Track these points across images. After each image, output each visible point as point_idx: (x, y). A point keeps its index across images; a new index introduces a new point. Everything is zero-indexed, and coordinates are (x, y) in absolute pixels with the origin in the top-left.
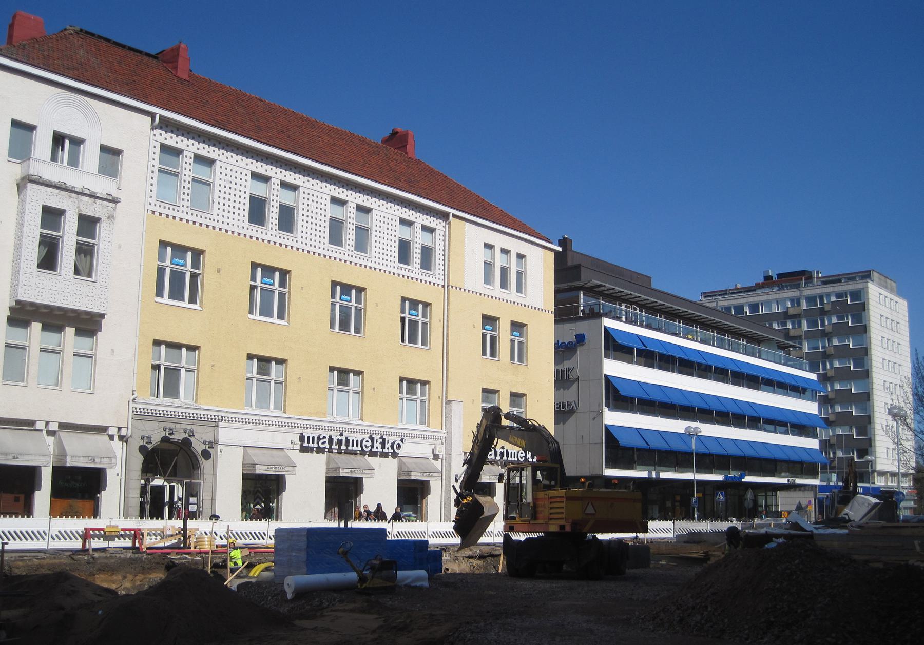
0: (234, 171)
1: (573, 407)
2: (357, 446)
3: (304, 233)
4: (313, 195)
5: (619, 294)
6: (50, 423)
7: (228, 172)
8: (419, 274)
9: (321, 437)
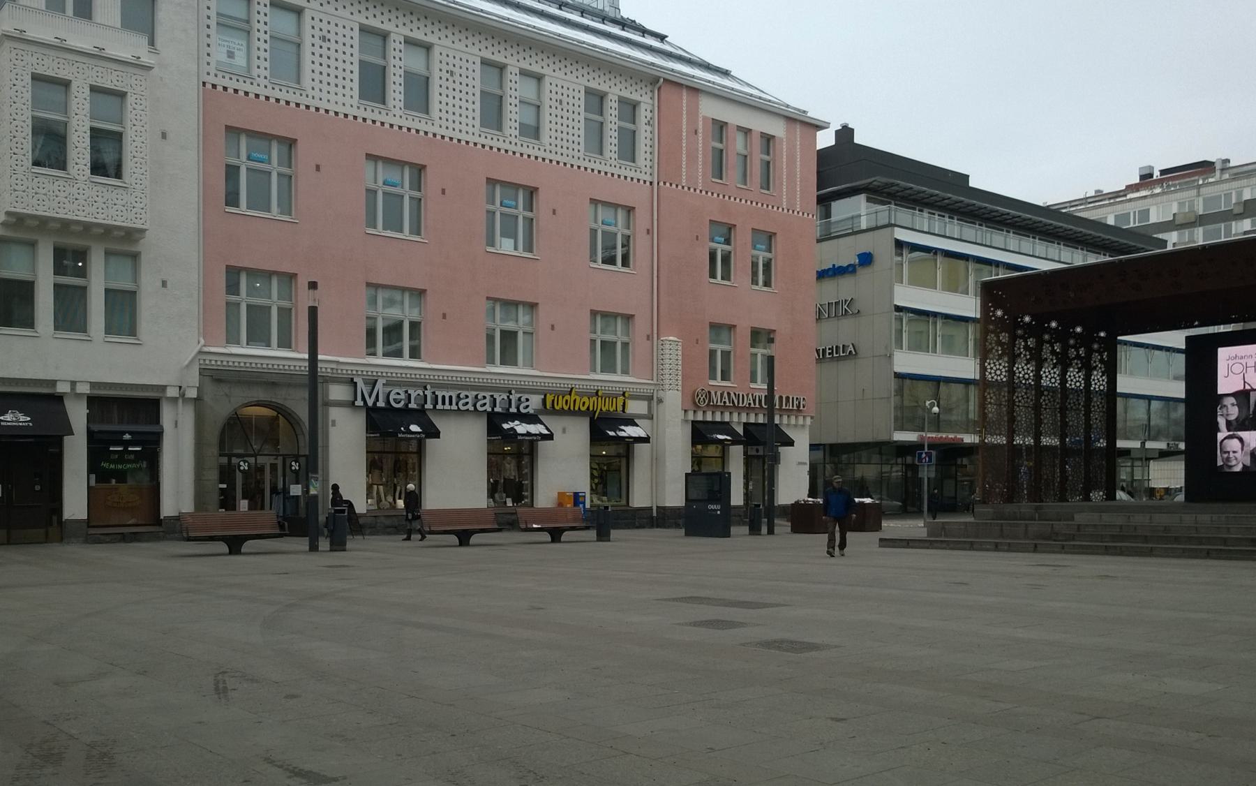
0: (325, 22)
1: (850, 351)
2: (451, 404)
3: (444, 111)
4: (562, 87)
5: (957, 204)
6: (168, 388)
7: (450, 60)
8: (615, 166)
9: (461, 396)
